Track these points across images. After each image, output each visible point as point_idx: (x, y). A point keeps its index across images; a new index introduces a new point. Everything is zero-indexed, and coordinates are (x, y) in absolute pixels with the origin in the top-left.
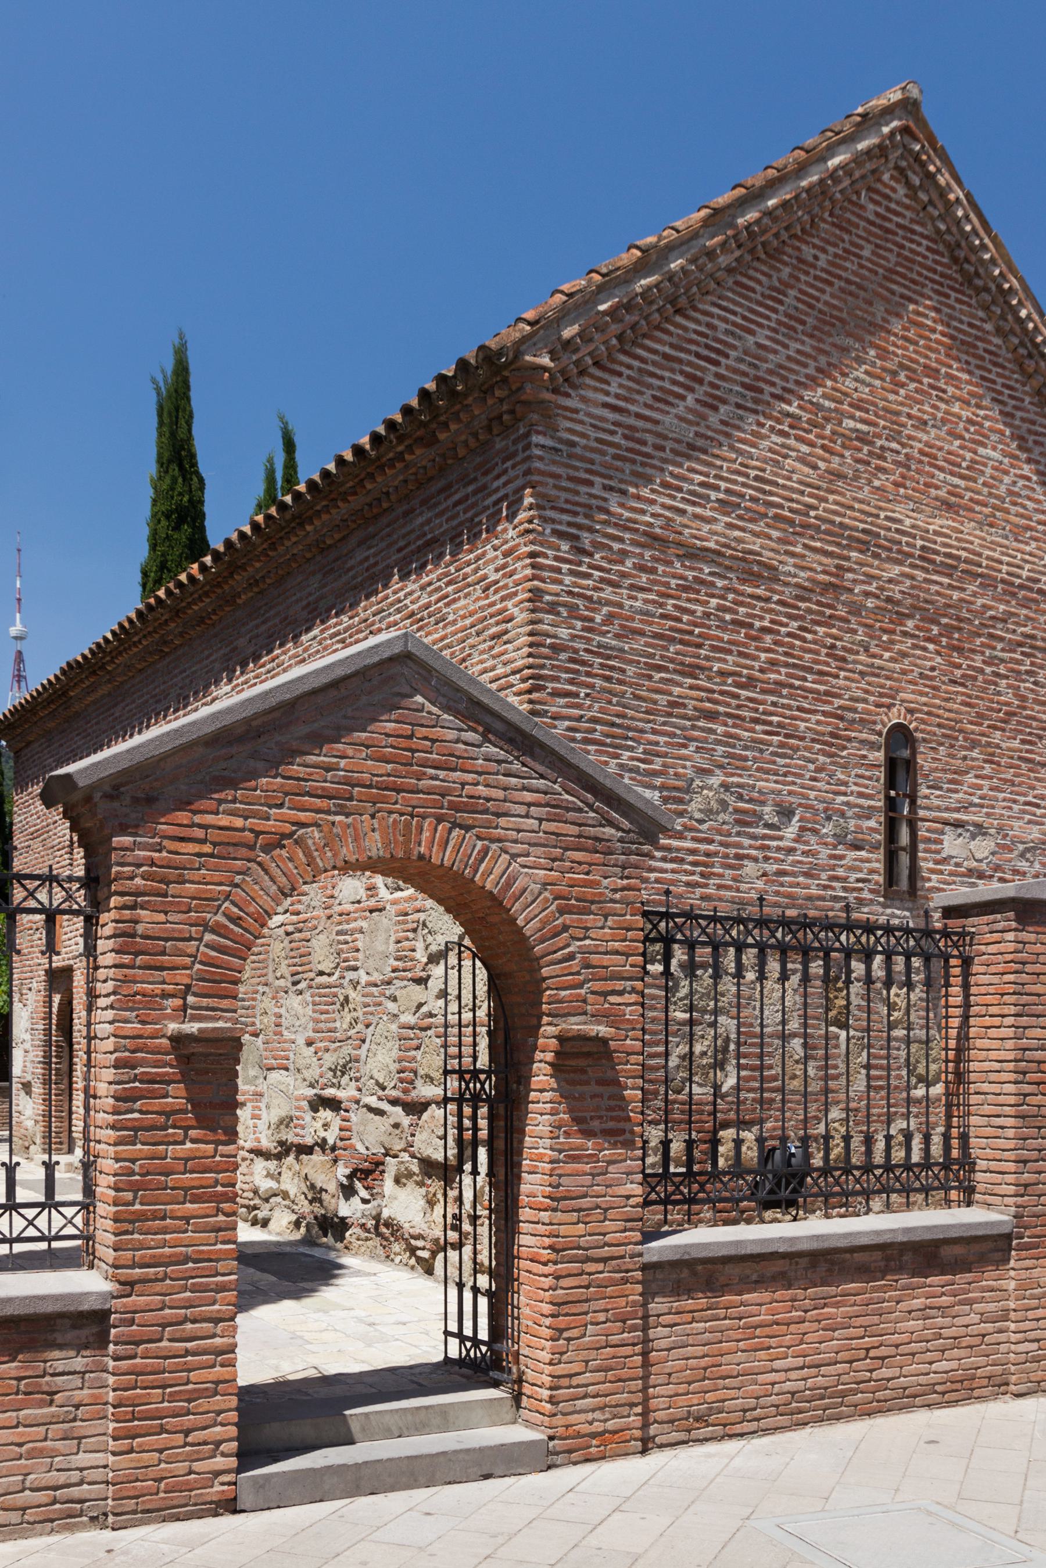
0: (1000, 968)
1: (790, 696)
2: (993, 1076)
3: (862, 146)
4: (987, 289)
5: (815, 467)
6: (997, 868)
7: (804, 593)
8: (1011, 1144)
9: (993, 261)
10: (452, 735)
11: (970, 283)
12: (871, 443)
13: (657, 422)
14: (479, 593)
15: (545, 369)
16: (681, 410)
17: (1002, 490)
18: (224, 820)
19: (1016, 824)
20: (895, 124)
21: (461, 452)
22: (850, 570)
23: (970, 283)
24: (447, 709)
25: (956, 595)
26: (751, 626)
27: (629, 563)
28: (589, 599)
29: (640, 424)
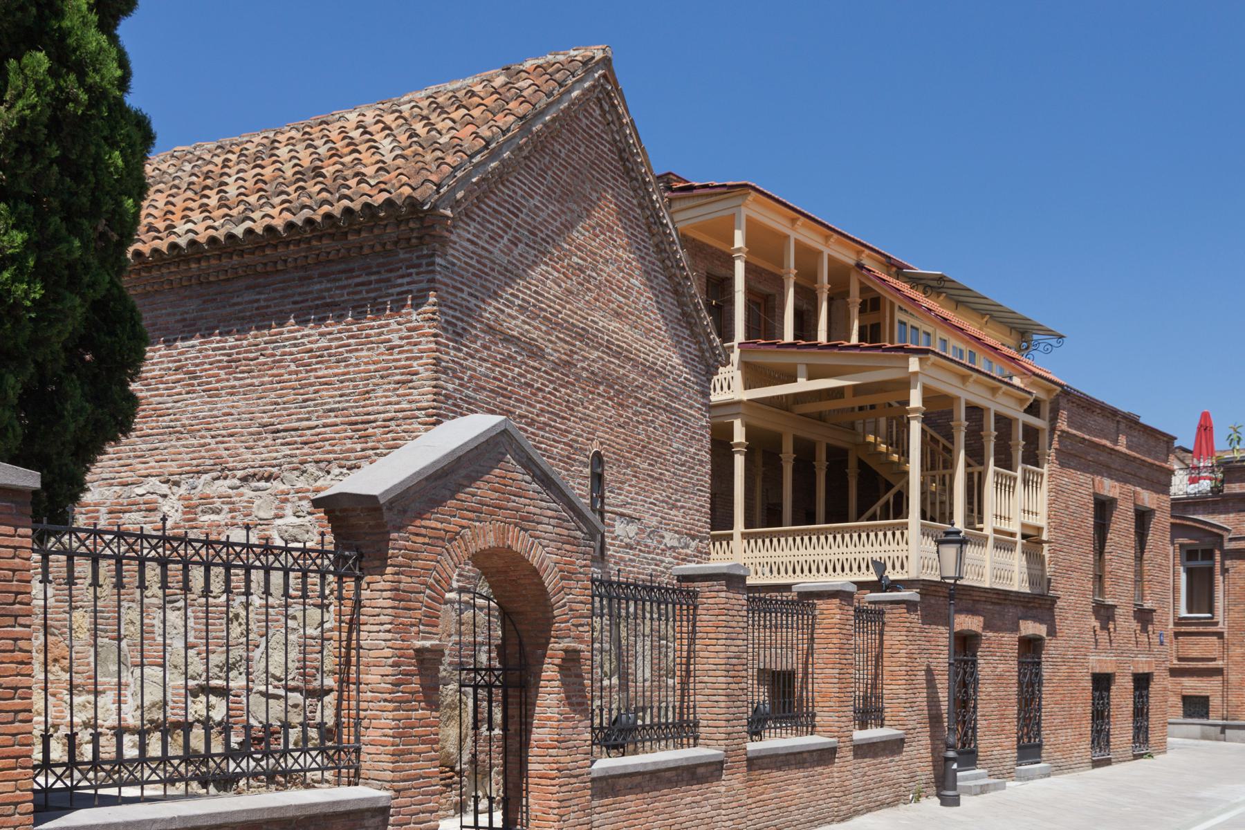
0: (717, 612)
1: (550, 432)
2: (711, 673)
3: (586, 85)
4: (637, 180)
5: (560, 286)
6: (638, 543)
7: (556, 366)
8: (723, 711)
9: (641, 163)
10: (520, 477)
11: (628, 174)
12: (584, 272)
13: (491, 253)
14: (382, 349)
15: (448, 217)
16: (500, 246)
17: (640, 306)
18: (433, 524)
19: (647, 516)
20: (600, 72)
21: (366, 251)
22: (576, 353)
23: (628, 174)
24: (519, 463)
25: (622, 371)
26: (532, 386)
27: (479, 343)
28: (461, 365)
29: (483, 253)
